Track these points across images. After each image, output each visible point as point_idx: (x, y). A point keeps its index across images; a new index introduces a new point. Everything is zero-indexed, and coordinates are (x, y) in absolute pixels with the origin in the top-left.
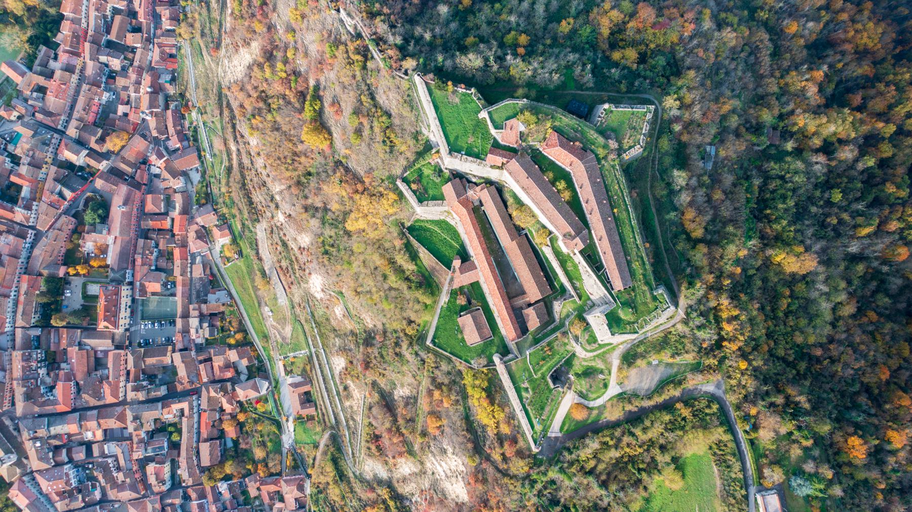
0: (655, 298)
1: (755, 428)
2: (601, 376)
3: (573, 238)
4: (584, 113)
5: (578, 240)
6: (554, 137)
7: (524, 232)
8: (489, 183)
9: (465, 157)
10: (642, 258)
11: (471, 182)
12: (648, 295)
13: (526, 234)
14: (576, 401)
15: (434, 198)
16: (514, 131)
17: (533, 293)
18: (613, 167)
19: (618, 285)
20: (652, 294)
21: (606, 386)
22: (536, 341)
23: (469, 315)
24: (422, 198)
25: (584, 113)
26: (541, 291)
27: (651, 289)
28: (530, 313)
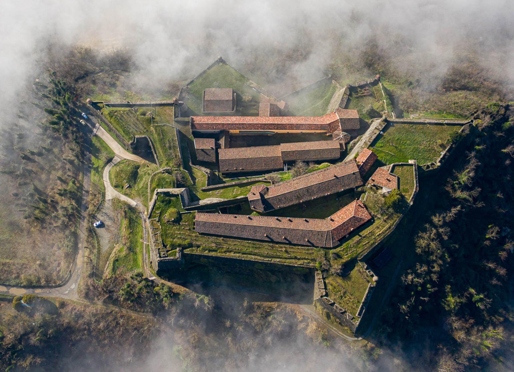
0: (173, 247)
1: (19, 307)
2: (127, 185)
3: (262, 195)
4: (376, 259)
5: (258, 197)
6: (365, 216)
7: (286, 168)
8: (344, 154)
9: (378, 133)
10: (216, 251)
11: (351, 140)
12: (179, 242)
13: (283, 170)
14: (115, 158)
15: (349, 100)
16: (385, 182)
17: (227, 154)
18: (314, 260)
19: (201, 217)
20: (179, 245)
21: (116, 187)
22: (182, 136)
23: (231, 98)
24: (352, 90)
25: (376, 259)
26: (225, 160)
27: (184, 247)
28: (208, 144)
